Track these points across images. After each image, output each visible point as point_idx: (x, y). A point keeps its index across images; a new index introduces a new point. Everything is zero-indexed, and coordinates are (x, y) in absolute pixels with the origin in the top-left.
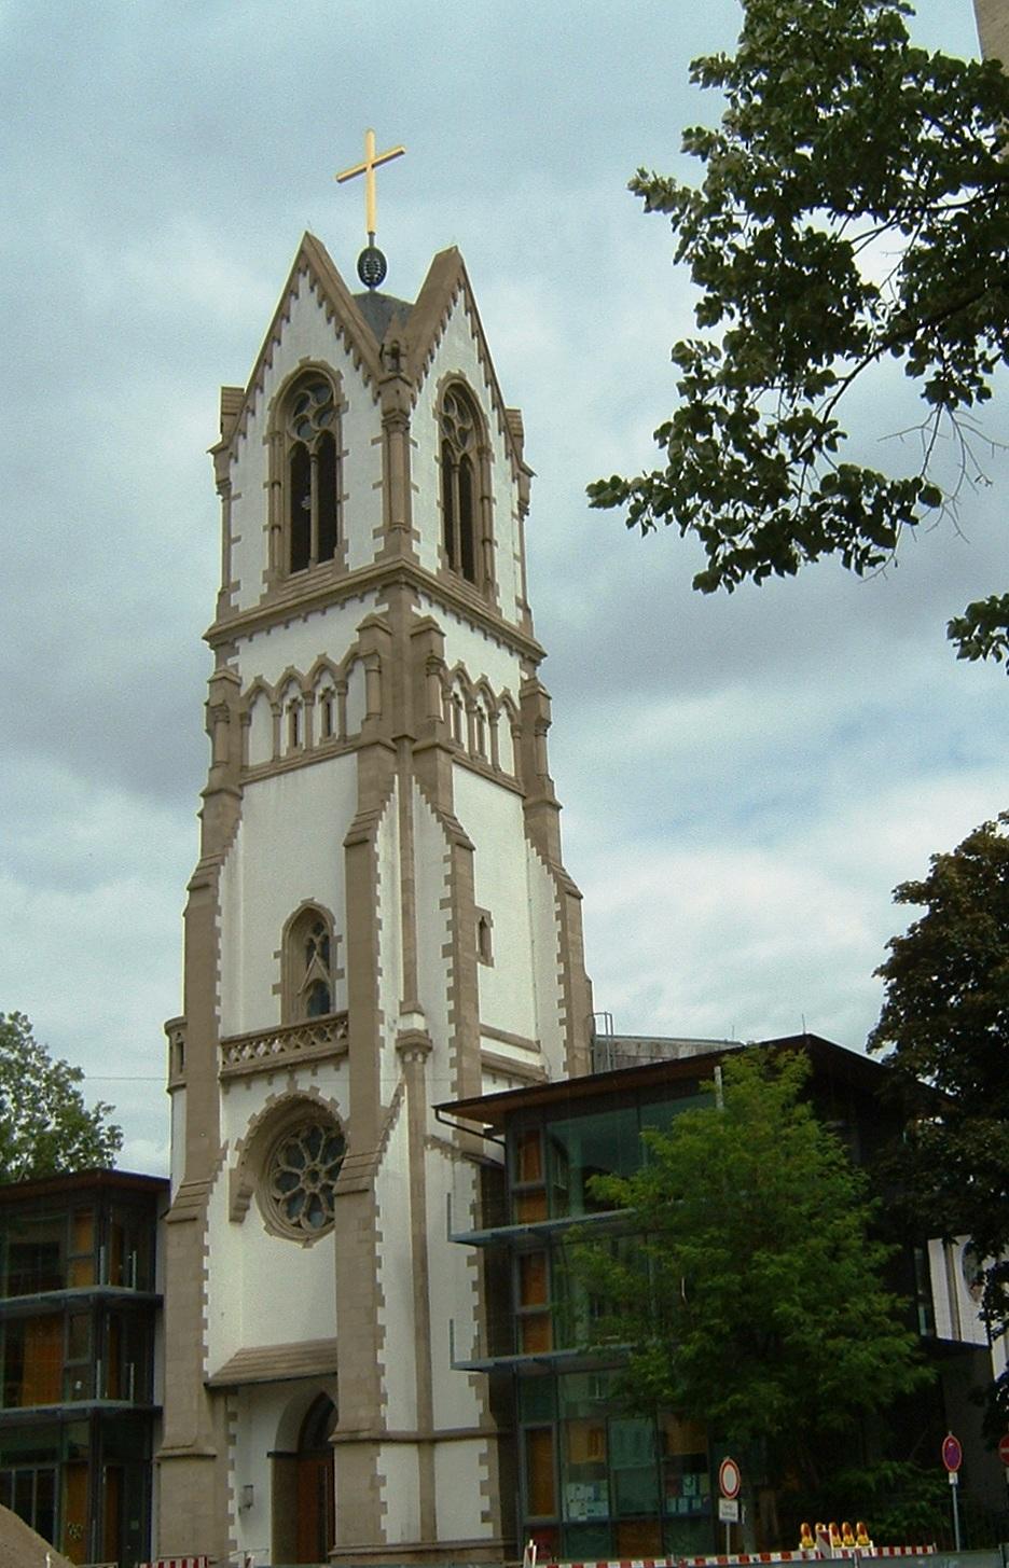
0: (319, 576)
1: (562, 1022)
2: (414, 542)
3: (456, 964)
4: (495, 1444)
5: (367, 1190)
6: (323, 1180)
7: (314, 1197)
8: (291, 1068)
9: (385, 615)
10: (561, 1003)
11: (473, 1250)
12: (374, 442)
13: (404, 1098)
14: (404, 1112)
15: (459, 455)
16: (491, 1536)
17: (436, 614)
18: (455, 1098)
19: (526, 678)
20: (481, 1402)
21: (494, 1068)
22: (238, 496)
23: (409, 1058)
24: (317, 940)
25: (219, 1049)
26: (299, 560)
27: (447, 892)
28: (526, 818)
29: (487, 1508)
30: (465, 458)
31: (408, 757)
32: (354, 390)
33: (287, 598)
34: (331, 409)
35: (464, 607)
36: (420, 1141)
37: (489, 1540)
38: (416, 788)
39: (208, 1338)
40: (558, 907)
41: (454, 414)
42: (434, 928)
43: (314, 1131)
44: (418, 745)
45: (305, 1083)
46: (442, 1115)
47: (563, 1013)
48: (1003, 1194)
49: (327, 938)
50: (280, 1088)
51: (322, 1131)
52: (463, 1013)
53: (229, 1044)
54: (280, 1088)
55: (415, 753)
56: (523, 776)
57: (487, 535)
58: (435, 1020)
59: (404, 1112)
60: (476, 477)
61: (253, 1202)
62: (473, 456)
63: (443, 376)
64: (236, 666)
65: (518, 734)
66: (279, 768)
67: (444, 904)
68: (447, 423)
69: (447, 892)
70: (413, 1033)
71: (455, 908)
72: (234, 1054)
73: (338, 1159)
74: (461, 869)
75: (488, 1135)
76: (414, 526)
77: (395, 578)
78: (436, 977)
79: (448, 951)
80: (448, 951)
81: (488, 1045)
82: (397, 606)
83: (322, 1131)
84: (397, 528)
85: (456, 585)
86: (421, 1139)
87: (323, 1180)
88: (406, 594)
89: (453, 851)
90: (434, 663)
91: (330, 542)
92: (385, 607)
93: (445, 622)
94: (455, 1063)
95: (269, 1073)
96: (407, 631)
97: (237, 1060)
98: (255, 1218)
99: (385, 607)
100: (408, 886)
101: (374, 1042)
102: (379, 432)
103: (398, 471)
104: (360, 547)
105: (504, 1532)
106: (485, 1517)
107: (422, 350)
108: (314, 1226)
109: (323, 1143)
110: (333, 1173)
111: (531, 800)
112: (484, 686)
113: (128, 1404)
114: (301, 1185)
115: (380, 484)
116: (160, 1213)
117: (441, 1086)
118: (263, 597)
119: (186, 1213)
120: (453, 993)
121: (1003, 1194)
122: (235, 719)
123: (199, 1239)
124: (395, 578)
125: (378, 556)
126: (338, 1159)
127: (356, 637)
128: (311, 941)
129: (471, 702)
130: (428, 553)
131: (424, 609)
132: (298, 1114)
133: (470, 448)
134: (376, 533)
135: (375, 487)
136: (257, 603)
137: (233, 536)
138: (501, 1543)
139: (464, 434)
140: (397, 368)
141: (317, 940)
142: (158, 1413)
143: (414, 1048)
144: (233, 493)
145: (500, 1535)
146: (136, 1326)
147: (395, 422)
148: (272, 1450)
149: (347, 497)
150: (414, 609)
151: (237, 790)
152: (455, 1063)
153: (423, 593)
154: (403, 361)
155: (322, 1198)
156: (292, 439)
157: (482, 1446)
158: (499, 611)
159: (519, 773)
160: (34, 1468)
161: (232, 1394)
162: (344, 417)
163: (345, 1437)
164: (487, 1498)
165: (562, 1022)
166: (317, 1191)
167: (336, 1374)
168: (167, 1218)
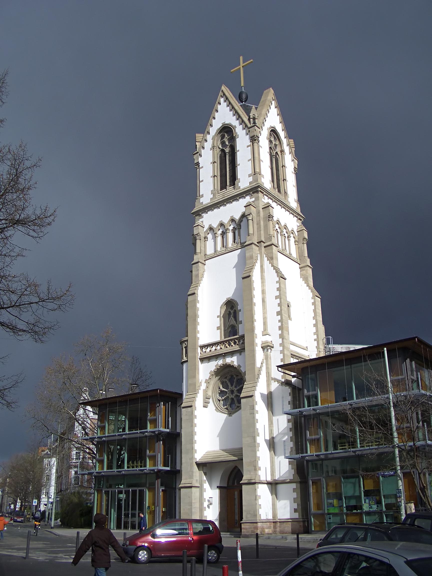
0: (230, 191)
1: (315, 340)
2: (262, 178)
3: (281, 318)
4: (299, 485)
5: (253, 396)
6: (236, 393)
7: (232, 399)
8: (224, 355)
9: (253, 202)
10: (315, 334)
11: (290, 417)
12: (248, 146)
13: (264, 365)
14: (264, 369)
15: (275, 152)
16: (298, 517)
17: (270, 201)
18: (282, 364)
19: (299, 225)
20: (293, 470)
21: (293, 356)
22: (202, 167)
23: (266, 350)
24: (232, 312)
25: (199, 348)
26: (223, 186)
27: (277, 293)
28: (301, 271)
29: (296, 507)
30: (277, 153)
31: (263, 249)
32: (240, 131)
33: (219, 198)
34: (233, 139)
35: (279, 201)
36: (269, 379)
37: (297, 519)
38: (266, 259)
39: (196, 446)
40: (313, 301)
41: (272, 139)
42: (273, 306)
43: (232, 376)
44: (265, 245)
45: (228, 360)
46: (280, 369)
47: (315, 337)
48: (5, 529)
49: (235, 311)
50: (220, 362)
51: (235, 376)
52: (284, 335)
53: (202, 347)
54: (220, 362)
55: (265, 247)
56: (299, 257)
57: (285, 178)
58: (274, 338)
59: (264, 369)
60: (280, 160)
61: (211, 400)
62: (279, 153)
63: (269, 127)
64: (202, 222)
65: (297, 243)
66: (216, 255)
67: (276, 297)
68: (271, 142)
69: (277, 293)
70: (267, 342)
71: (280, 299)
72: (204, 350)
73: (241, 386)
74: (282, 286)
75: (294, 376)
76: (262, 173)
77: (255, 190)
78: (274, 322)
79: (279, 313)
80: (279, 313)
81: (292, 348)
82: (257, 199)
83: (235, 376)
84: (256, 173)
85: (275, 192)
86: (270, 379)
87: (236, 393)
88: (260, 194)
89: (279, 279)
90: (270, 217)
91: (234, 178)
92: (253, 199)
93: (274, 204)
94: (282, 352)
95: (216, 357)
96: (261, 207)
97: (205, 352)
98: (211, 405)
99: (253, 199)
100: (263, 292)
101: (253, 344)
102: (249, 143)
103: (256, 155)
104: (244, 181)
105: (303, 516)
106: (295, 510)
107: (262, 118)
108: (232, 409)
109: (235, 380)
110: (240, 391)
111: (301, 266)
112: (286, 227)
113: (168, 469)
114: (236, 389)
115: (250, 160)
116: (178, 405)
117: (276, 358)
118: (211, 199)
119: (189, 404)
120: (281, 328)
121: (5, 529)
122: (202, 239)
123: (192, 413)
124: (255, 190)
125: (250, 183)
126: (241, 386)
127: (244, 209)
128: (230, 312)
129: (282, 231)
130: (266, 182)
131: (266, 200)
132: (227, 370)
133: (278, 150)
134: (249, 176)
135: (249, 161)
136: (209, 201)
137: (200, 180)
138: (301, 520)
139: (276, 145)
140: (254, 123)
141: (232, 312)
142: (179, 472)
143: (266, 347)
144: (200, 167)
145: (301, 517)
146: (173, 441)
147: (254, 139)
148: (219, 485)
149: (239, 165)
150: (263, 200)
151: (204, 262)
152: (282, 352)
153: (266, 195)
154: (256, 120)
155: (235, 400)
156: (219, 148)
157: (294, 486)
158: (289, 203)
159: (298, 256)
160: (138, 489)
161: (206, 467)
162: (237, 140)
163: (246, 481)
164: (296, 504)
165: (315, 340)
166: (233, 397)
167: (242, 460)
168: (182, 406)
